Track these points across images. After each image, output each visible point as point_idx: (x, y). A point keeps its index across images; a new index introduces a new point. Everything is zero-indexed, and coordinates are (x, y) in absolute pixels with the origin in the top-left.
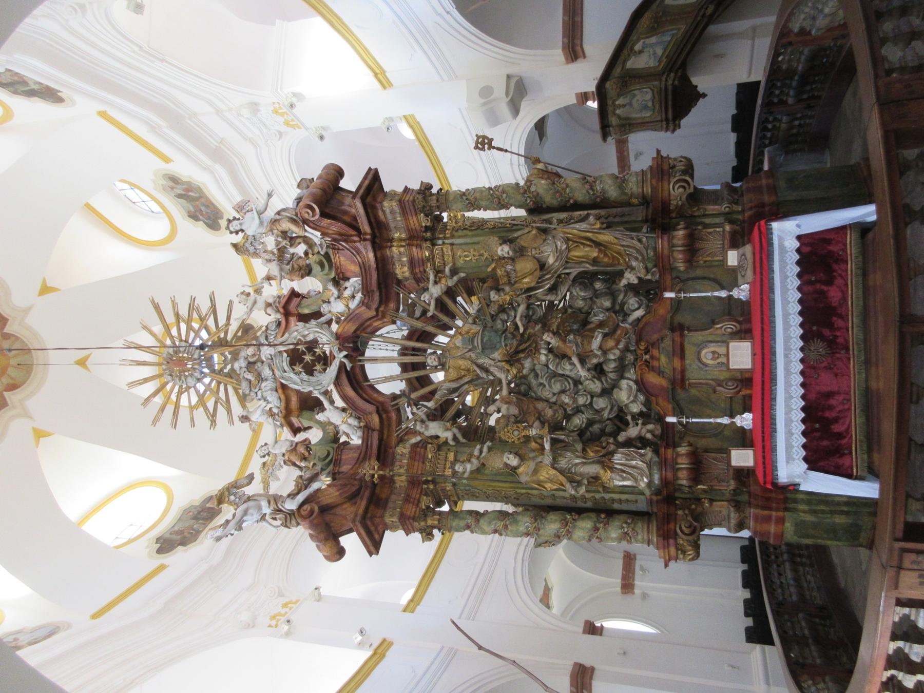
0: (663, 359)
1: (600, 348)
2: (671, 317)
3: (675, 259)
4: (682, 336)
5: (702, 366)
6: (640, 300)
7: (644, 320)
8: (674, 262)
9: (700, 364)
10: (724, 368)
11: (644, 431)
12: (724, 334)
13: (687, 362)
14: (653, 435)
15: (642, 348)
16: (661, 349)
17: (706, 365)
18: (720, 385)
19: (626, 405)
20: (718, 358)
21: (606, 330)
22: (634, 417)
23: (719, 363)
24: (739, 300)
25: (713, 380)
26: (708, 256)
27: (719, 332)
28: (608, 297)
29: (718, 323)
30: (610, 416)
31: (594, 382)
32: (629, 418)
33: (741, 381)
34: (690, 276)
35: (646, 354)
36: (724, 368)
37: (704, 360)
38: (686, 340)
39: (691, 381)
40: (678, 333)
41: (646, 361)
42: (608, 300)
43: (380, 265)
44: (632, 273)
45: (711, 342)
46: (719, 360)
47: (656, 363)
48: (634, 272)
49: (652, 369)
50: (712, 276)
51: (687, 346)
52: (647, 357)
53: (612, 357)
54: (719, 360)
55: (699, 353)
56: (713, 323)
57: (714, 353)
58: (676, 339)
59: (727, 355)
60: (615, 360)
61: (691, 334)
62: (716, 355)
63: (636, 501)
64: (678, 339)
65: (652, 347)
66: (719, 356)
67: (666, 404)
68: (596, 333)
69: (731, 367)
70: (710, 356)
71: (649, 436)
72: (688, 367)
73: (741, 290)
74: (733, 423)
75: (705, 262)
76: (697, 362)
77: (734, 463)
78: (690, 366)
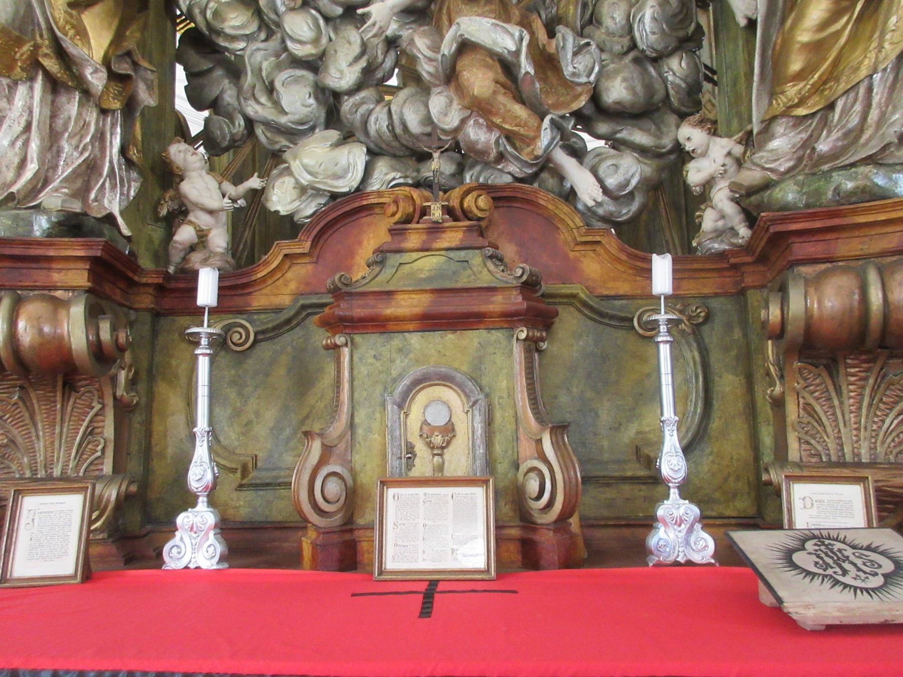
0: (428, 264)
1: (465, 46)
2: (574, 296)
3: (816, 282)
4: (510, 319)
5: (400, 388)
6: (631, 194)
7: (563, 209)
8: (807, 282)
9: (406, 381)
10: (393, 464)
11: (202, 219)
12: (517, 467)
13: (415, 340)
14: (192, 248)
15: (469, 202)
16: (462, 254)
17: (402, 404)
18: (327, 452)
19: (288, 171)
20: (431, 446)
21: (526, 67)
22: (256, 196)
23: (410, 449)
24: (649, 523)
25: (352, 425)
26: (809, 409)
27: (526, 448)
28: (639, 89)
29: (556, 445)
30: (259, 131)
31: (357, 59)
32: (254, 182)
33: (348, 525)
34: (715, 357)
35: (448, 211)
36: (393, 464)
37: (422, 398)
38: (497, 335)
39: (346, 351)
40: (516, 301)
41: (425, 211)
42: (631, 89)
43: (567, 488)
44: (729, 161)
45: (489, 422)
46: (420, 448)
47: (414, 240)
48: (732, 168)
49: (397, 231)
50: (715, 424)
51: (473, 338)
52: (436, 213)
53: (437, 102)
54: (420, 448)
55: (446, 379)
56: (559, 429)
57: (449, 430)
58: (499, 298)
59: (438, 480)
60: (428, 120)
61: (518, 352)
62: (438, 440)
63: (804, 499)
64: (497, 304)
65: (469, 229)
66: (439, 450)
67: (293, 286)
68: (516, 30)
69: (391, 492)
70: (438, 418)
71: (185, 234)
72: (397, 341)
73: (691, 530)
74: (188, 501)
75: (778, 404)
76: (416, 371)
77: (31, 504)
78: (400, 350)
